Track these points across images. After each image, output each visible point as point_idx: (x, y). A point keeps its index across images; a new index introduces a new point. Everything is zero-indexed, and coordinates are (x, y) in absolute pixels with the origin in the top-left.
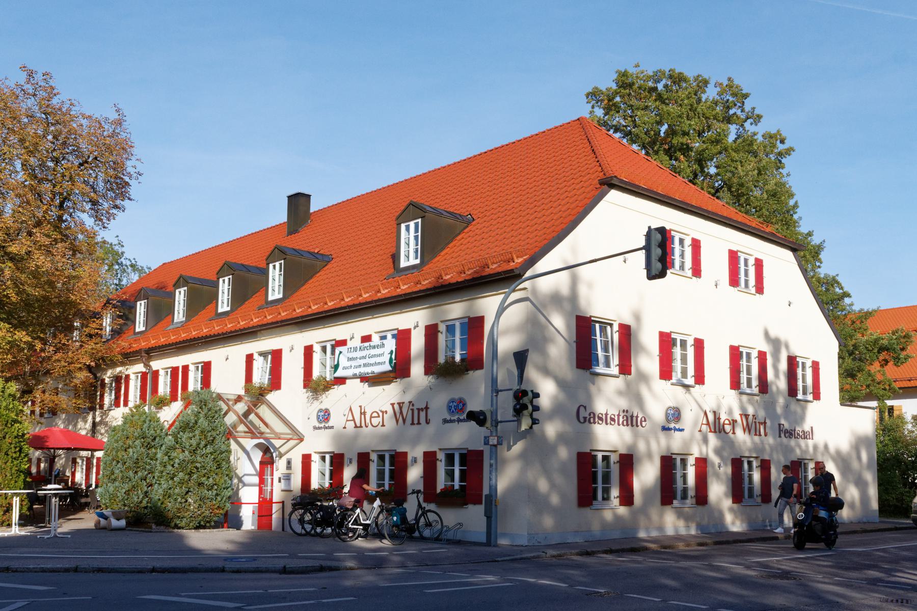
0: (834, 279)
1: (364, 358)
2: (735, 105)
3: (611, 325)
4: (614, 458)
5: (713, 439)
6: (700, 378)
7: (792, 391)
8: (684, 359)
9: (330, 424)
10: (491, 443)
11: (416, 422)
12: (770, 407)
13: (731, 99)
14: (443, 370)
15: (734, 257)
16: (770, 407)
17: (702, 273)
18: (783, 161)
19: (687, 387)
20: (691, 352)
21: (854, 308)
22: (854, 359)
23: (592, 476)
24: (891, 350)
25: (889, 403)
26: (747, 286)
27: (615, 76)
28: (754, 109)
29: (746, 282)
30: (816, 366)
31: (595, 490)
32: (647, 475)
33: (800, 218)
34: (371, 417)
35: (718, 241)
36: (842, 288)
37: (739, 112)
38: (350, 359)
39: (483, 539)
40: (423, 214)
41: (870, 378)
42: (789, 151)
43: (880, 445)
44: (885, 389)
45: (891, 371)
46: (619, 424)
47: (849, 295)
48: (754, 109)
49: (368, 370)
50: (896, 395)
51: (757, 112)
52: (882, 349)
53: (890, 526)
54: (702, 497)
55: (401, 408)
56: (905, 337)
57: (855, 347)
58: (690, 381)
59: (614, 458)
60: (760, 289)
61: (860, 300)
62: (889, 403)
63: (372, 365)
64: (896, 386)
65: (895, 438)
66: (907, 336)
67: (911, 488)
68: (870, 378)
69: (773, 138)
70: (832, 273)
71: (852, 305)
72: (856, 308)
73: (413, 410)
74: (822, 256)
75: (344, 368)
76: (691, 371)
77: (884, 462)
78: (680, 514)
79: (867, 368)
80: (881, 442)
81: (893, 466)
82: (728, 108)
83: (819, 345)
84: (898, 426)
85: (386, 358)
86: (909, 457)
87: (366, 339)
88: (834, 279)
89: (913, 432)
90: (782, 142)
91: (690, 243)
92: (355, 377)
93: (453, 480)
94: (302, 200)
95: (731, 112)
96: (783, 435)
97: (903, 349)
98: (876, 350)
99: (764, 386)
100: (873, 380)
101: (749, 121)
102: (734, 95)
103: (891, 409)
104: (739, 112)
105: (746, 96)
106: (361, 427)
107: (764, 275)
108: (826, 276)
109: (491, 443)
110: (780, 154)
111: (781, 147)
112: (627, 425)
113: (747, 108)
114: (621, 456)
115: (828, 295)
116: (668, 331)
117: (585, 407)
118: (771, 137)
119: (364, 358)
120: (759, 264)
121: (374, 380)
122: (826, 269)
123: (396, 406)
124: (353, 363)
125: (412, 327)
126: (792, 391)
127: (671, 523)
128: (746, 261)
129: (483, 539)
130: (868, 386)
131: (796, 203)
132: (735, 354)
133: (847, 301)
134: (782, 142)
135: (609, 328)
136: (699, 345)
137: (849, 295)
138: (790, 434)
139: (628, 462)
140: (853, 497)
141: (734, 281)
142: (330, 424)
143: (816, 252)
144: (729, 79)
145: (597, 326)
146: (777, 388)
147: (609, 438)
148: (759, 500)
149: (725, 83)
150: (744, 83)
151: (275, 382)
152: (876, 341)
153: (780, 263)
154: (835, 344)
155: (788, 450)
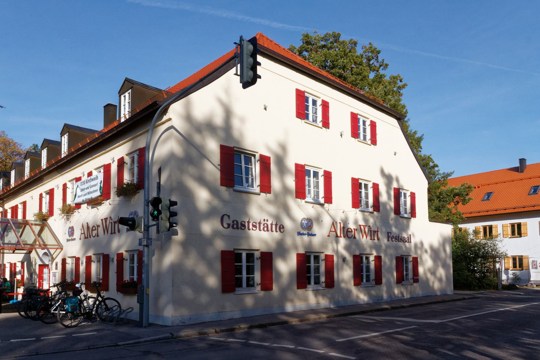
0: (429, 157)
1: (88, 188)
2: (373, 58)
3: (254, 156)
4: (257, 254)
5: (343, 241)
6: (328, 199)
7: (397, 211)
8: (317, 186)
9: (74, 237)
10: (143, 244)
11: (113, 232)
12: (385, 220)
13: (370, 54)
14: (126, 192)
15: (355, 118)
16: (385, 220)
17: (330, 125)
18: (401, 91)
19: (322, 205)
20: (321, 180)
21: (440, 172)
22: (440, 201)
23: (238, 267)
24: (461, 195)
25: (460, 226)
26: (365, 138)
27: (302, 37)
28: (383, 60)
29: (365, 137)
30: (413, 195)
31: (310, 277)
32: (286, 267)
33: (409, 120)
34: (92, 230)
35: (342, 105)
36: (433, 162)
37: (376, 63)
38: (82, 190)
39: (137, 318)
40: (132, 85)
41: (449, 211)
42: (404, 86)
43: (454, 248)
44: (457, 218)
45: (461, 208)
46: (260, 230)
47: (437, 166)
48: (383, 60)
49: (89, 197)
50: (464, 221)
51: (385, 62)
52: (456, 195)
53: (461, 297)
54: (330, 283)
55: (106, 222)
56: (468, 187)
57: (441, 193)
58: (322, 201)
59: (257, 254)
60: (374, 141)
61: (443, 166)
62: (460, 226)
63: (91, 193)
64: (464, 216)
65: (463, 243)
66: (469, 187)
67: (472, 273)
68: (449, 211)
69: (395, 79)
70: (428, 154)
71: (439, 170)
72: (441, 172)
73: (111, 223)
74: (422, 144)
75: (79, 197)
76: (322, 194)
77: (457, 258)
78: (316, 292)
79: (448, 206)
80: (455, 246)
81: (462, 259)
82: (370, 60)
83: (416, 184)
84: (464, 237)
85: (98, 187)
86: (471, 254)
87: (90, 174)
88: (429, 157)
89: (473, 240)
90: (401, 81)
91: (321, 103)
92: (83, 202)
93: (133, 275)
94: (111, 108)
95: (371, 62)
96: (390, 240)
97: (467, 195)
98: (452, 196)
99: (377, 206)
100: (451, 213)
101: (382, 68)
102: (372, 52)
103: (460, 229)
104: (376, 63)
105: (379, 52)
106: (87, 238)
107: (377, 132)
108: (425, 156)
109: (143, 244)
110: (399, 88)
111: (400, 84)
112: (268, 230)
113: (380, 60)
114: (262, 253)
115: (426, 165)
116: (303, 164)
117: (229, 216)
118: (394, 78)
119: (88, 188)
120: (373, 125)
121: (94, 203)
122: (425, 152)
123: (104, 221)
124: (83, 193)
125: (111, 162)
126: (397, 211)
127: (311, 299)
128: (364, 122)
129: (137, 318)
130: (448, 216)
131: (407, 110)
132: (356, 185)
133: (436, 169)
134: (401, 81)
135: (253, 158)
136: (328, 176)
137: (437, 166)
138: (399, 239)
139: (267, 259)
140: (441, 276)
141: (355, 134)
142: (74, 237)
143: (419, 140)
144: (370, 44)
145: (242, 156)
146: (390, 211)
147: (260, 239)
148: (374, 283)
149: (368, 46)
150: (377, 45)
151: (51, 212)
152: (452, 190)
153: (387, 126)
154: (426, 182)
155: (397, 248)
